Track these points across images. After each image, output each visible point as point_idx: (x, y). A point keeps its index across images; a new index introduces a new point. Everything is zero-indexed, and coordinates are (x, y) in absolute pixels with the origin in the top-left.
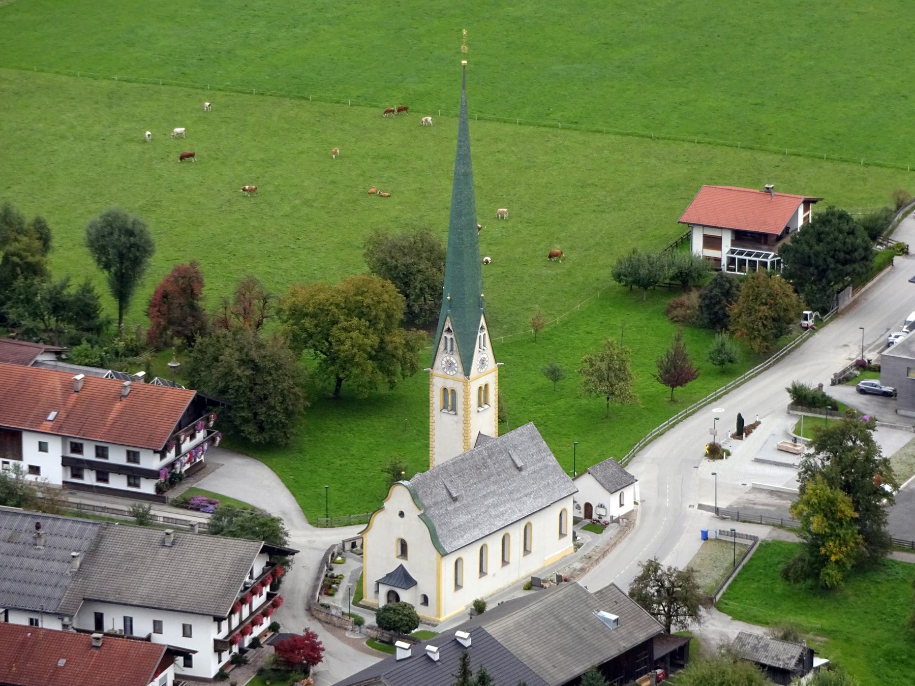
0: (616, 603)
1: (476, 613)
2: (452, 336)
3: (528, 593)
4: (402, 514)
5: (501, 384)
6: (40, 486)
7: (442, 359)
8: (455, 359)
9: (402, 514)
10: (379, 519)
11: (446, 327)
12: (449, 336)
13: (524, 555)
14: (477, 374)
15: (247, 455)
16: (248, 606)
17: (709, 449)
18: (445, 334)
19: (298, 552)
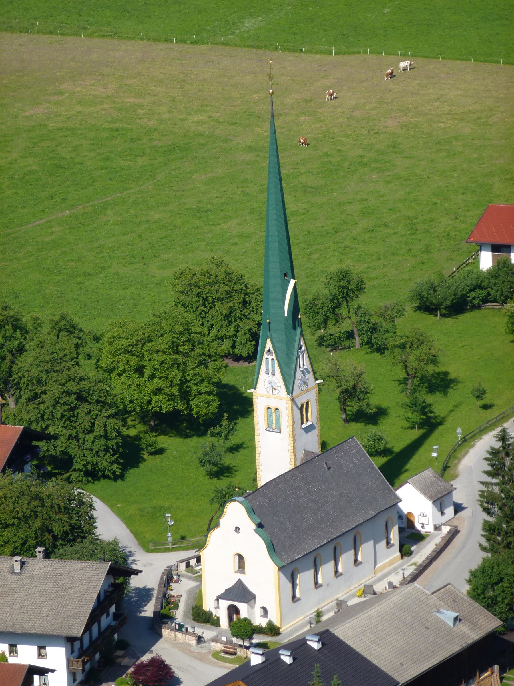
0: (455, 602)
1: (198, 604)
2: (274, 357)
3: (362, 599)
4: (237, 529)
5: (320, 401)
6: (159, 587)
7: (263, 380)
8: (278, 378)
9: (237, 529)
10: (214, 536)
11: (267, 349)
12: (270, 357)
13: (464, 508)
14: (299, 392)
15: (295, 642)
16: (96, 624)
17: (167, 665)
18: (265, 356)
19: (141, 571)
